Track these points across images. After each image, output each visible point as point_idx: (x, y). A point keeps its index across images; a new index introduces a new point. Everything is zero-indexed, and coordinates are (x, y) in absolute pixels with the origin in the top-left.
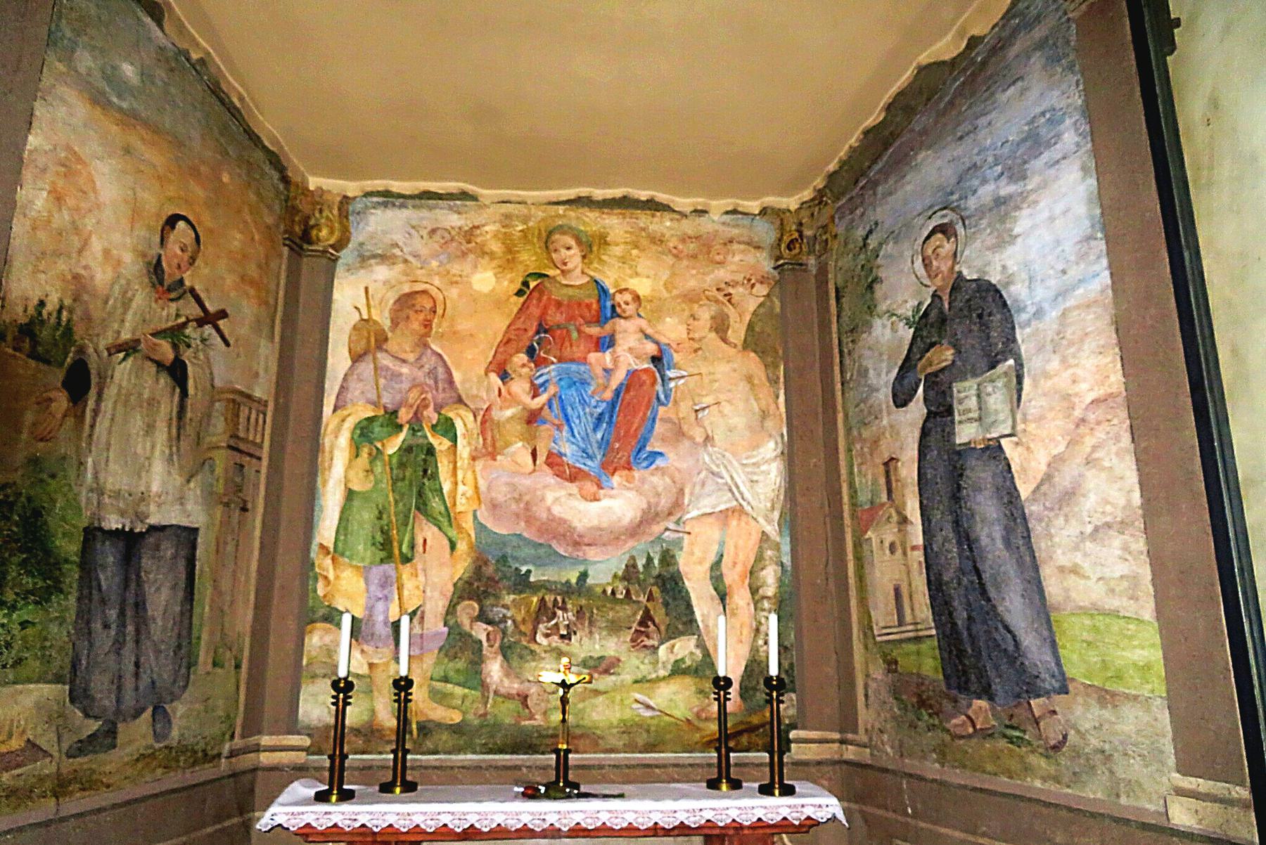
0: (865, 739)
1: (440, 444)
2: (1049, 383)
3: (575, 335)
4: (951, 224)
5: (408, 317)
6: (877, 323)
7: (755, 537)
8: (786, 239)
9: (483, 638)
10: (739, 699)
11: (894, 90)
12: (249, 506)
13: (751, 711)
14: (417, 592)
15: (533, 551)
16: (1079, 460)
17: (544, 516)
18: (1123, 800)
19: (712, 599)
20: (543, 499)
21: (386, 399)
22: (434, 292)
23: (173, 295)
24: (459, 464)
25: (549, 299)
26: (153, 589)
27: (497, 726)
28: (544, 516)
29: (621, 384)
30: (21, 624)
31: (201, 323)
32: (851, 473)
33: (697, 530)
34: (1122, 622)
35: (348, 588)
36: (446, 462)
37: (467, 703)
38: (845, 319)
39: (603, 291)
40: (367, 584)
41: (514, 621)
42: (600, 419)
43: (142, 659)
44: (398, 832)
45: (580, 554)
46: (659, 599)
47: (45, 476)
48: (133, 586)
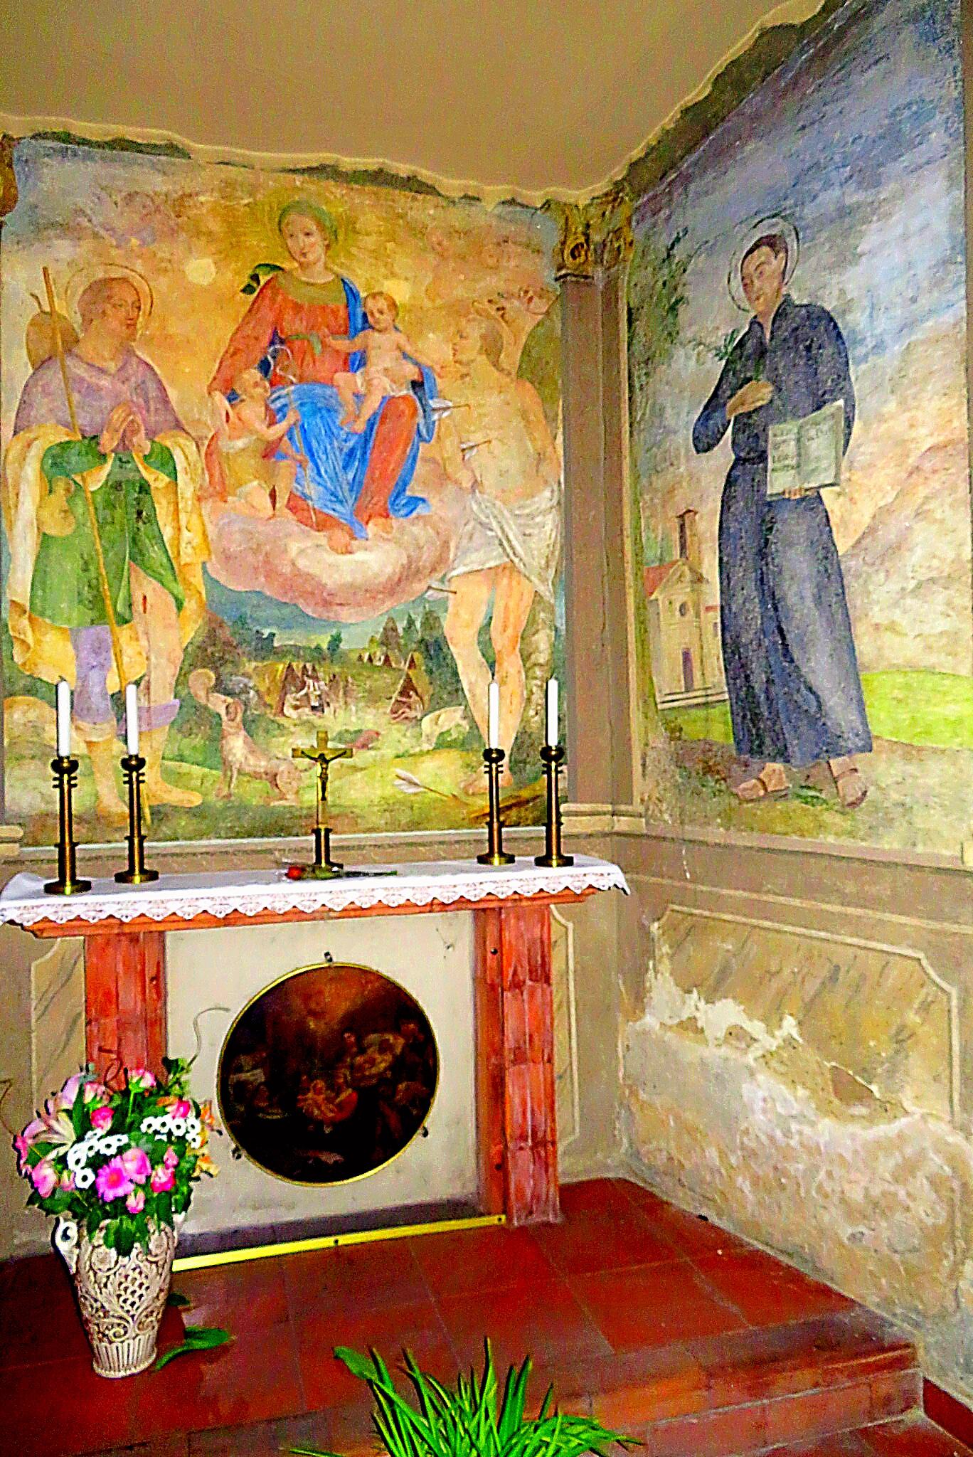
0: (641, 809)
1: (157, 480)
2: (885, 426)
3: (318, 348)
4: (781, 237)
5: (104, 312)
6: (680, 353)
7: (528, 599)
8: (571, 244)
9: (223, 712)
13: (521, 785)
14: (138, 659)
15: (276, 612)
16: (910, 511)
17: (287, 570)
18: (920, 849)
19: (481, 666)
20: (285, 551)
21: (83, 420)
22: (137, 281)
25: (285, 299)
27: (243, 809)
29: (375, 414)
32: (638, 527)
33: (464, 589)
34: (937, 678)
36: (164, 502)
37: (207, 784)
38: (637, 348)
39: (352, 294)
40: (76, 647)
41: (257, 691)
42: (351, 453)
45: (332, 615)
46: (422, 665)
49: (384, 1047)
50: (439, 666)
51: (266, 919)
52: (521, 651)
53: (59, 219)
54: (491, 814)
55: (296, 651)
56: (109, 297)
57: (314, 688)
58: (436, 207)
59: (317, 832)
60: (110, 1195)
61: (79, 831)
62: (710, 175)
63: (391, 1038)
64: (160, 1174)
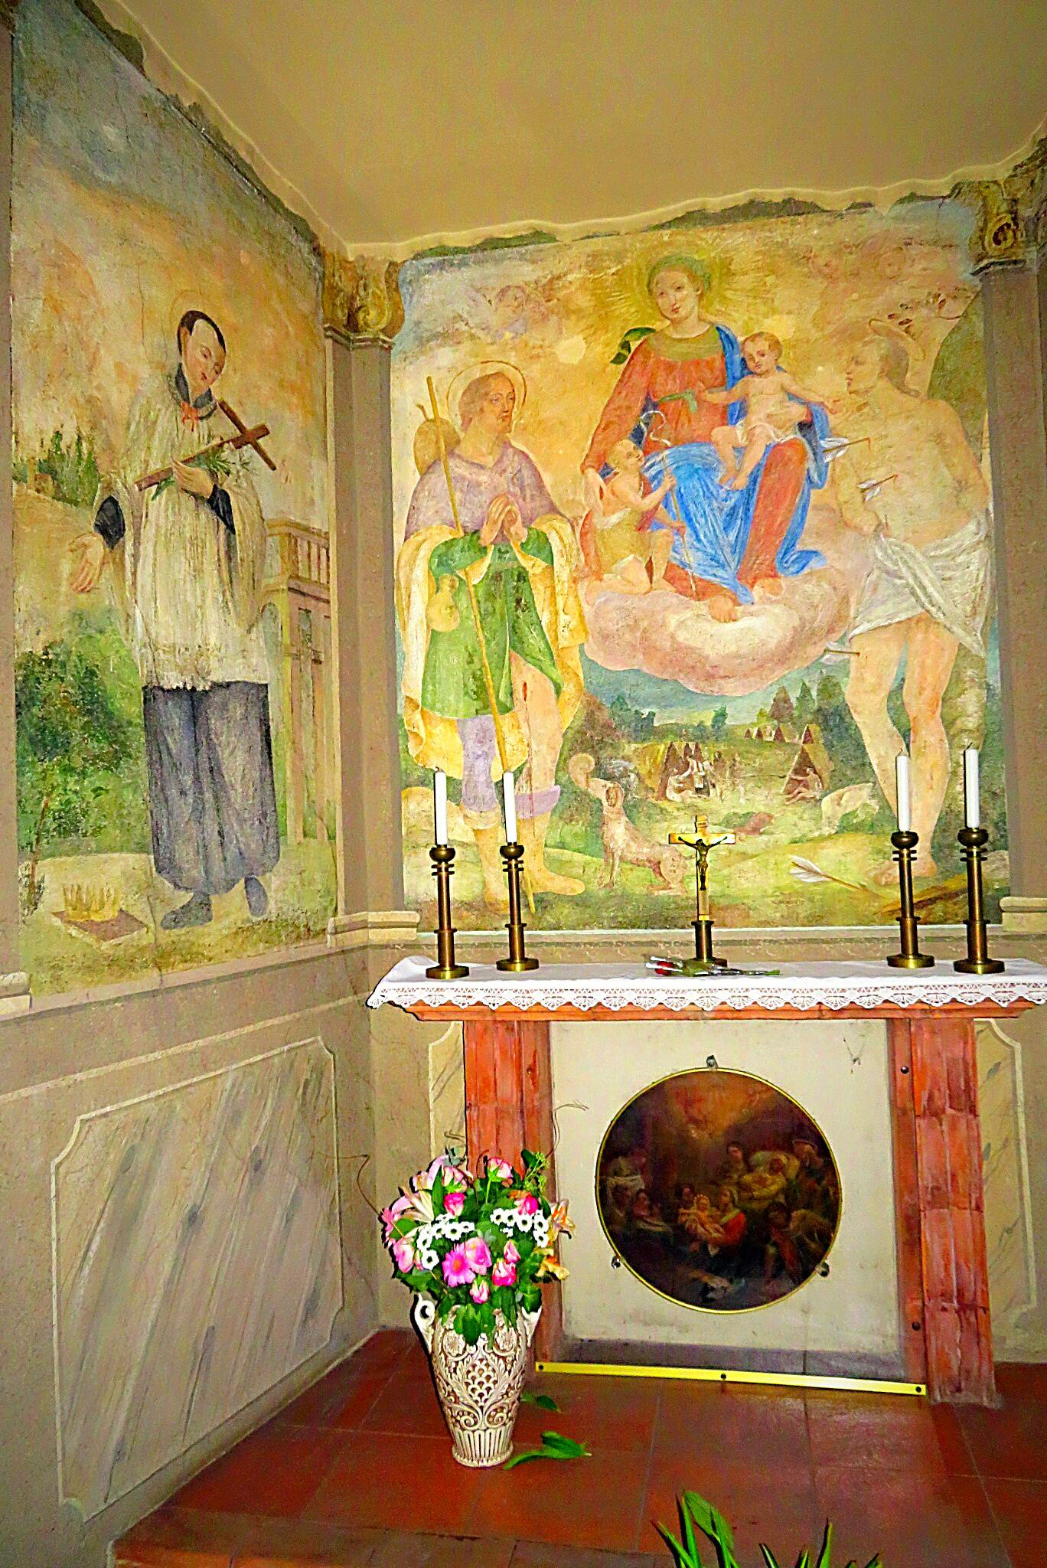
1: (533, 566)
5: (482, 410)
7: (948, 657)
8: (993, 227)
9: (604, 799)
10: (930, 859)
12: (322, 657)
15: (655, 690)
20: (663, 625)
21: (465, 518)
22: (511, 372)
23: (203, 412)
24: (558, 589)
25: (658, 362)
26: (227, 752)
27: (625, 898)
30: (94, 791)
31: (239, 443)
35: (440, 744)
36: (541, 587)
37: (590, 871)
39: (728, 341)
40: (463, 737)
42: (732, 514)
43: (226, 829)
44: (518, 1011)
45: (716, 689)
46: (820, 739)
47: (92, 632)
48: (204, 749)
49: (776, 1168)
50: (841, 738)
51: (629, 1016)
53: (440, 329)
54: (903, 909)
55: (677, 731)
56: (487, 394)
57: (699, 769)
58: (820, 225)
59: (697, 925)
60: (454, 1280)
63: (783, 1159)
64: (501, 1267)
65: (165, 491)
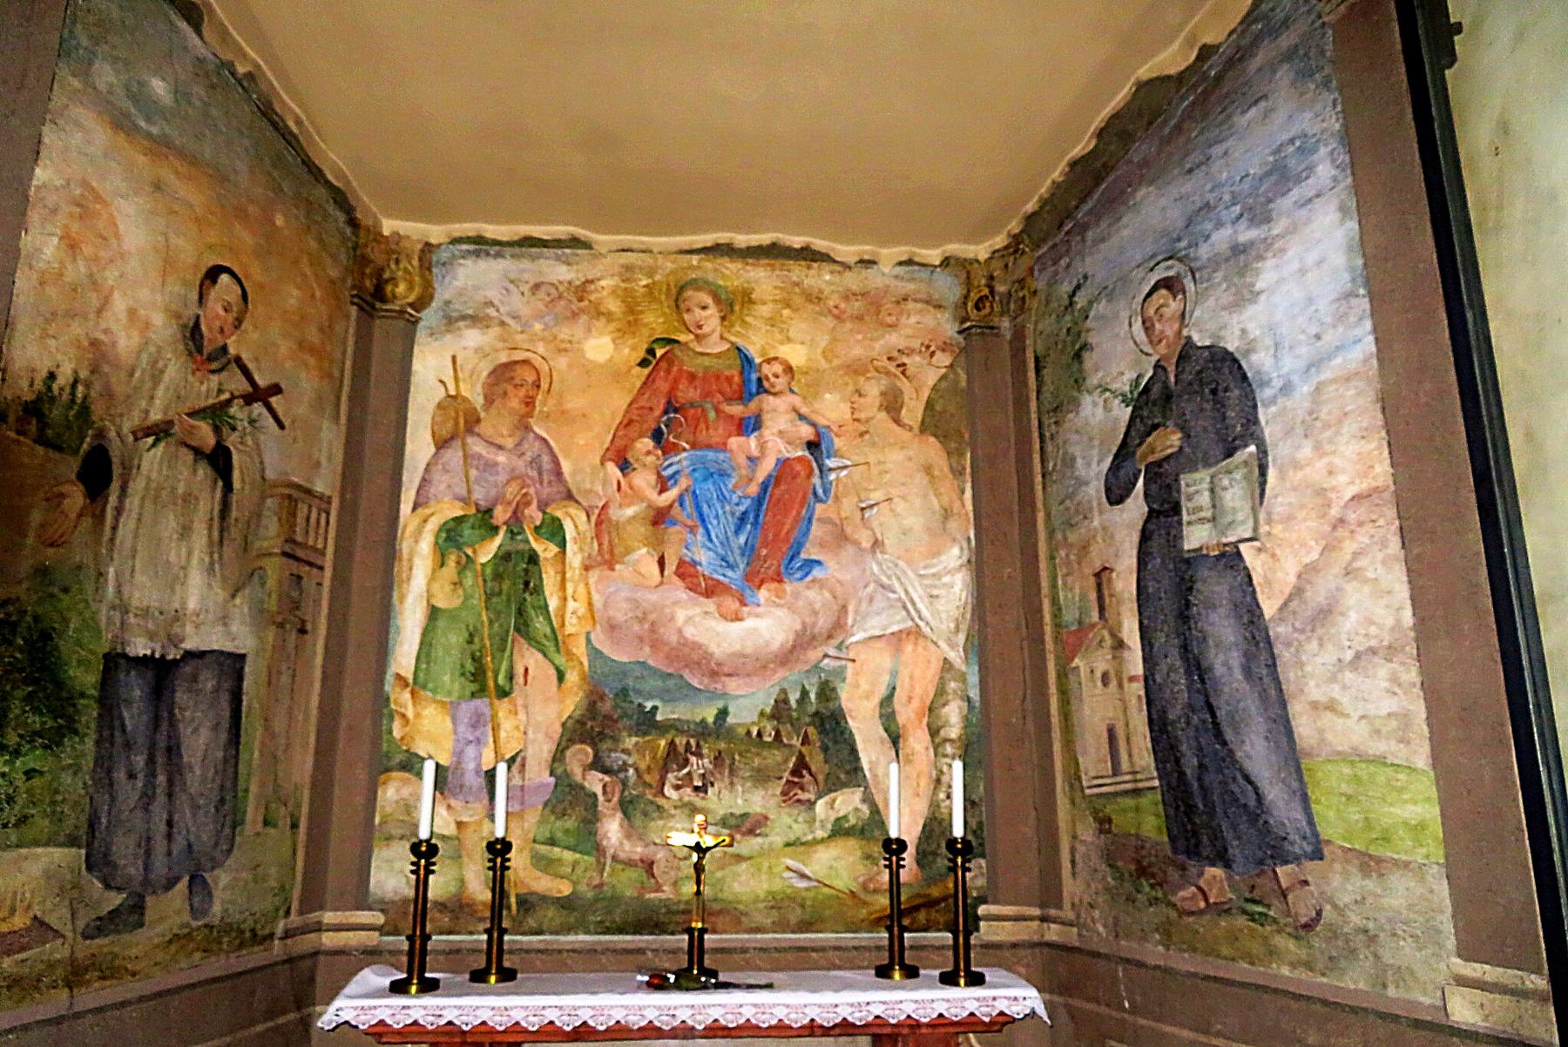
0: (1071, 915)
1: (545, 550)
2: (1300, 475)
3: (712, 415)
5: (505, 393)
6: (1087, 400)
7: (936, 666)
8: (974, 296)
10: (915, 866)
11: (1107, 112)
12: (309, 627)
13: (930, 881)
14: (516, 734)
15: (660, 683)
16: (1337, 570)
17: (674, 639)
18: (1391, 992)
19: (882, 742)
20: (672, 619)
21: (479, 495)
22: (537, 361)
23: (214, 366)
25: (680, 370)
27: (616, 899)
28: (674, 639)
29: (770, 476)
30: (26, 773)
31: (249, 400)
32: (1054, 586)
33: (863, 657)
35: (430, 728)
36: (552, 573)
37: (579, 871)
38: (1046, 395)
39: (747, 361)
41: (636, 770)
42: (743, 519)
43: (176, 817)
44: (493, 1031)
45: (719, 686)
46: (816, 742)
48: (164, 726)
52: (929, 726)
57: (698, 766)
61: (434, 919)
62: (1104, 225)
65: (163, 444)
